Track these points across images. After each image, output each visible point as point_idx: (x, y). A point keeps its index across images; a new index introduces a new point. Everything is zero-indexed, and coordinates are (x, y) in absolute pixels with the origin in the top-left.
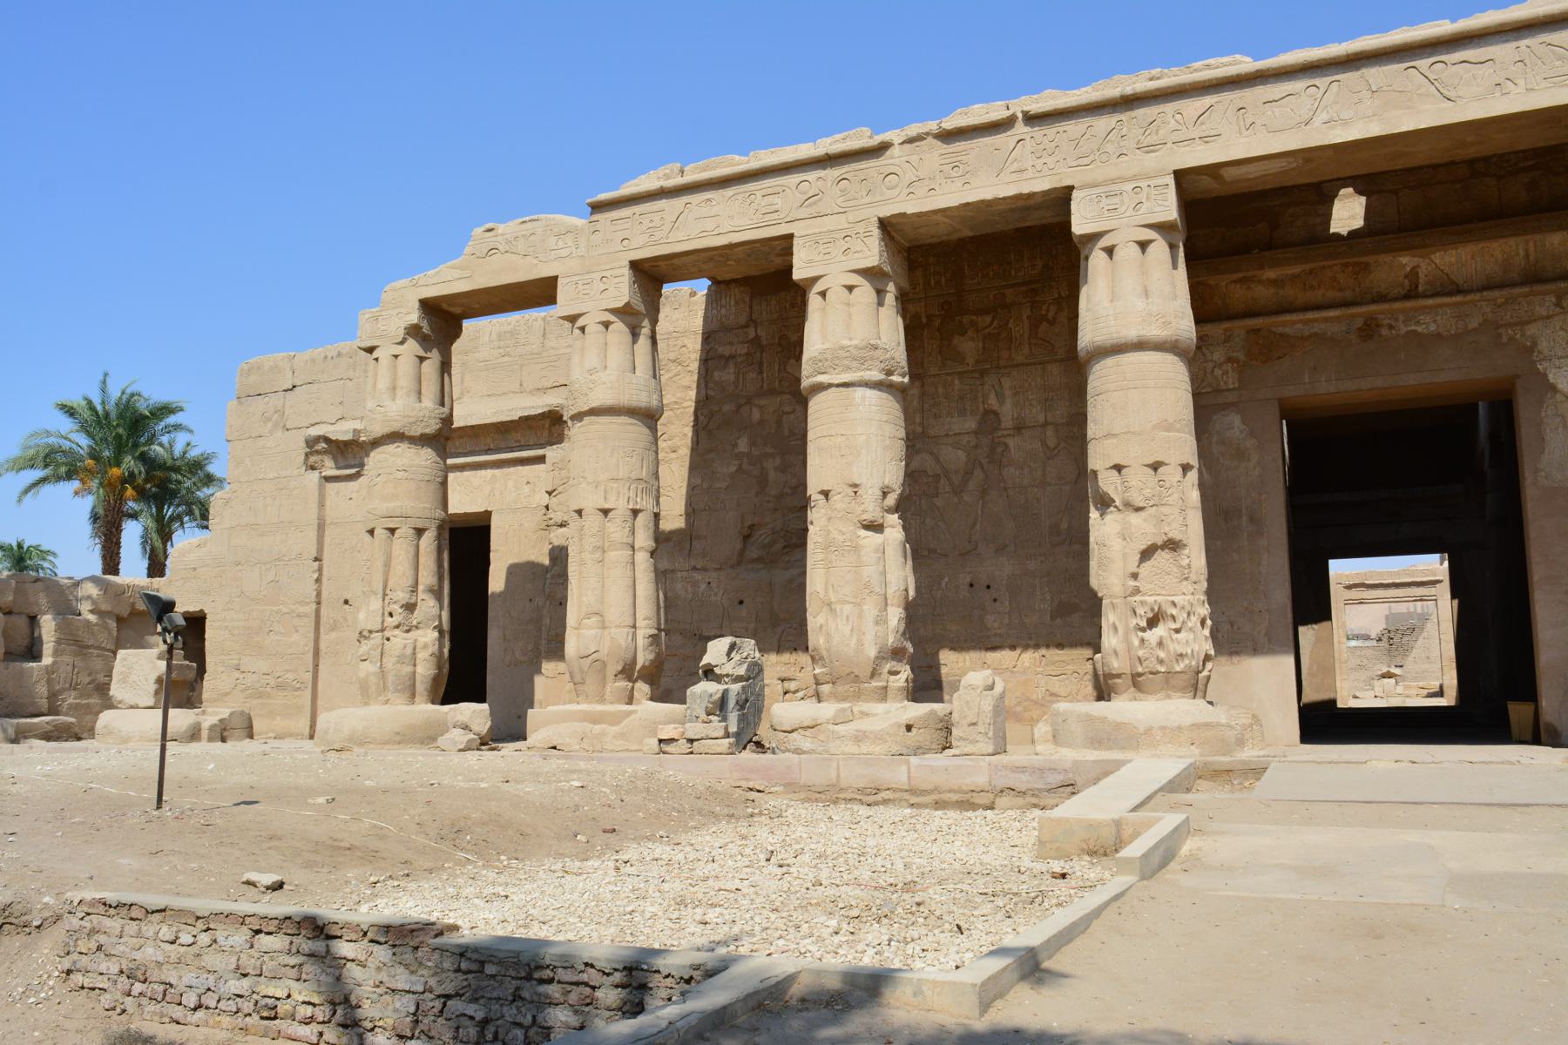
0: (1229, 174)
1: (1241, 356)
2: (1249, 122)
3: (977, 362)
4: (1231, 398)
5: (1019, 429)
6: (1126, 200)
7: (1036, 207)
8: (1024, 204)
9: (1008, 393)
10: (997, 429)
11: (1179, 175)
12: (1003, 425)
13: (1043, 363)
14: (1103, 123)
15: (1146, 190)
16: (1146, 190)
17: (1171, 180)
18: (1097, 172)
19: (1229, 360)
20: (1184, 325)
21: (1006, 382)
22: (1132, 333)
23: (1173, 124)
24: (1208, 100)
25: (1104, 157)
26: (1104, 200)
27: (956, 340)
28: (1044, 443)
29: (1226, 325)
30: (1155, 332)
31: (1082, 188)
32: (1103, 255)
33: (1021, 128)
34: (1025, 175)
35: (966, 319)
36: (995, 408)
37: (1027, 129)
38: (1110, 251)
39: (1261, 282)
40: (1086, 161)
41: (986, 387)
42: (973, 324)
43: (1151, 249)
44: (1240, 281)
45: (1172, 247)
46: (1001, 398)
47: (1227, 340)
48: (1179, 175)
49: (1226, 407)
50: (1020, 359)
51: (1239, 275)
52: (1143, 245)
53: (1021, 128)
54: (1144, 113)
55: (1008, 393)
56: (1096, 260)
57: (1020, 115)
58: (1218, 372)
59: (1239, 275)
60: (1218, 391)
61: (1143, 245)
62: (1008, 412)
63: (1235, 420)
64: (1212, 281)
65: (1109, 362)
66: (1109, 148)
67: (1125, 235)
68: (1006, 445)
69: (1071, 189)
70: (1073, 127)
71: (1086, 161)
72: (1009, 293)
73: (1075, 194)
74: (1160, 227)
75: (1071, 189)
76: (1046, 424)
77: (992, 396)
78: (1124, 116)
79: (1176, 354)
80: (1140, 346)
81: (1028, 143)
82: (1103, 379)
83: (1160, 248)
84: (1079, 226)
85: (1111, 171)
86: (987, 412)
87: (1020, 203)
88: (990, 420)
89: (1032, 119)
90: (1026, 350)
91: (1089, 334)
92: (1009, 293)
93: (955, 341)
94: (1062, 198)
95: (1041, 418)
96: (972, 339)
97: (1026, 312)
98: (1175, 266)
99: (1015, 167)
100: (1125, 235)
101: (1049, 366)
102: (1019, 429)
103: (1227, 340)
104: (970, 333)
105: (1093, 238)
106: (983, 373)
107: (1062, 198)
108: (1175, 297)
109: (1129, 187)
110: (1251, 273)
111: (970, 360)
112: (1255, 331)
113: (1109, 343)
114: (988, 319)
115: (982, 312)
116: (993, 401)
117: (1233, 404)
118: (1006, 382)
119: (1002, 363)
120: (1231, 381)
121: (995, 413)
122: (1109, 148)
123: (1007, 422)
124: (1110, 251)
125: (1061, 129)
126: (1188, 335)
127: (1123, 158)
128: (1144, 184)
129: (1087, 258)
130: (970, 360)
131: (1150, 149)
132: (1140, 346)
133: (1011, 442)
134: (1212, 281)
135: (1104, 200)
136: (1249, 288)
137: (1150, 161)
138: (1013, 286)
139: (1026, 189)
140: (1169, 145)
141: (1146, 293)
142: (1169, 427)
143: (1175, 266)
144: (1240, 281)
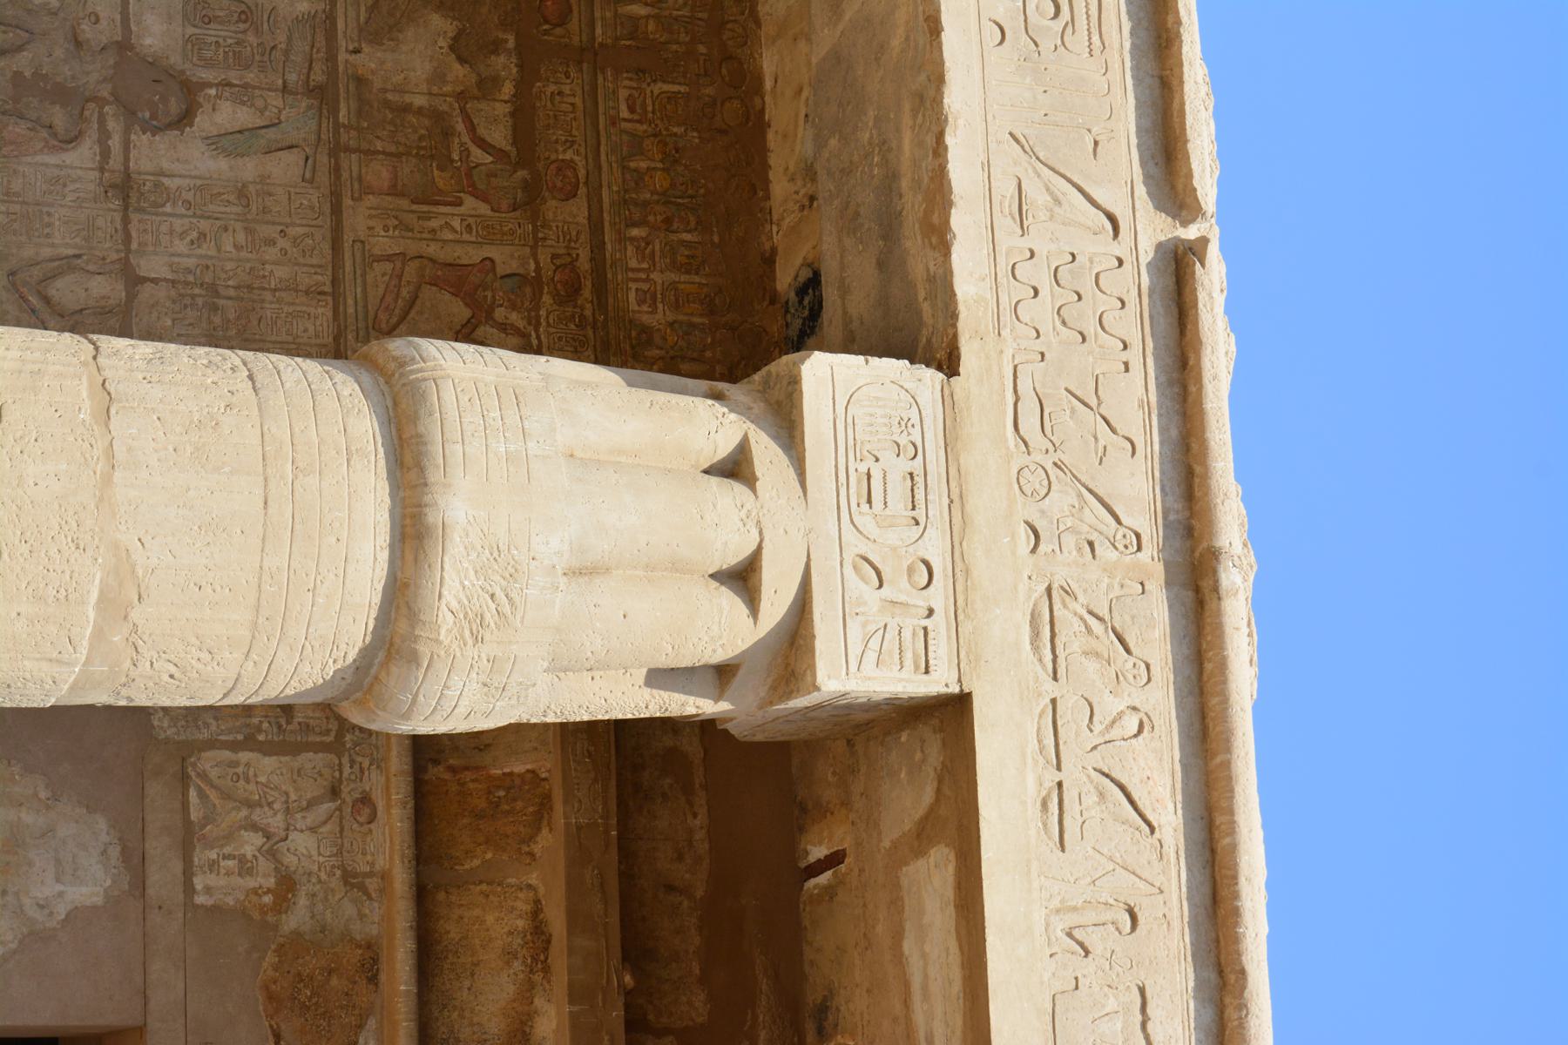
0: (932, 876)
1: (296, 919)
2: (1092, 938)
3: (360, 81)
4: (162, 878)
5: (124, 189)
6: (892, 537)
7: (889, 262)
8: (906, 209)
9: (249, 169)
10: (130, 114)
11: (952, 713)
12: (141, 140)
13: (337, 292)
14: (1138, 488)
15: (921, 601)
16: (921, 601)
17: (940, 683)
18: (990, 456)
19: (287, 885)
20: (460, 695)
21: (285, 167)
22: (458, 506)
23: (1110, 705)
24: (1171, 819)
25: (1035, 481)
26: (904, 465)
27: (440, 25)
28: (68, 265)
29: (401, 880)
30: (454, 582)
31: (948, 401)
32: (724, 446)
33: (1152, 229)
34: (1006, 224)
35: (504, 65)
36: (203, 122)
37: (1147, 253)
38: (736, 468)
39: (527, 991)
40: (1029, 423)
41: (275, 100)
42: (487, 86)
43: (729, 601)
44: (538, 929)
45: (722, 675)
46: (226, 143)
47: (351, 879)
48: (952, 713)
49: (135, 862)
50: (358, 219)
51: (557, 922)
52: (743, 578)
53: (1152, 229)
54: (1154, 621)
55: (249, 169)
56: (707, 422)
57: (1191, 233)
58: (251, 844)
59: (557, 922)
60: (187, 839)
61: (743, 578)
62: (182, 159)
63: (90, 885)
64: (549, 843)
65: (366, 427)
66: (1062, 499)
67: (781, 520)
68: (72, 140)
69: (949, 365)
70: (1135, 395)
71: (1029, 423)
72: (578, 211)
73: (930, 377)
74: (795, 636)
75: (949, 365)
76: (135, 281)
77: (244, 117)
78: (1151, 560)
79: (367, 654)
80: (412, 532)
81: (1099, 249)
82: (319, 408)
83: (729, 630)
84: (825, 376)
85: (990, 496)
86: (190, 92)
87: (912, 205)
88: (171, 100)
89: (1178, 267)
90: (383, 243)
91: (466, 378)
92: (578, 211)
93: (437, 21)
94: (918, 332)
95: (152, 265)
96: (438, 76)
97: (506, 258)
98: (660, 677)
99: (1036, 195)
100: (781, 520)
101: (324, 312)
102: (124, 189)
103: (351, 879)
104: (458, 70)
105: (786, 421)
106: (322, 95)
107: (918, 332)
108: (559, 668)
109: (935, 548)
110: (559, 959)
111: (370, 60)
112: (371, 967)
113: (432, 430)
114: (499, 136)
115: (522, 115)
116: (225, 115)
117: (140, 884)
118: (285, 167)
119: (351, 163)
120: (218, 884)
121: (185, 119)
122: (1062, 499)
123: (154, 154)
124: (736, 468)
125: (1134, 356)
126: (426, 702)
127: (1024, 540)
128: (938, 596)
129: (718, 397)
130: (370, 60)
131: (1045, 629)
132: (412, 532)
133: (82, 156)
134: (549, 843)
135: (904, 465)
136: (510, 955)
137: (1005, 624)
138: (596, 226)
139: (964, 222)
140: (1050, 689)
141: (585, 571)
142: (113, 607)
143: (660, 677)
144: (538, 929)
